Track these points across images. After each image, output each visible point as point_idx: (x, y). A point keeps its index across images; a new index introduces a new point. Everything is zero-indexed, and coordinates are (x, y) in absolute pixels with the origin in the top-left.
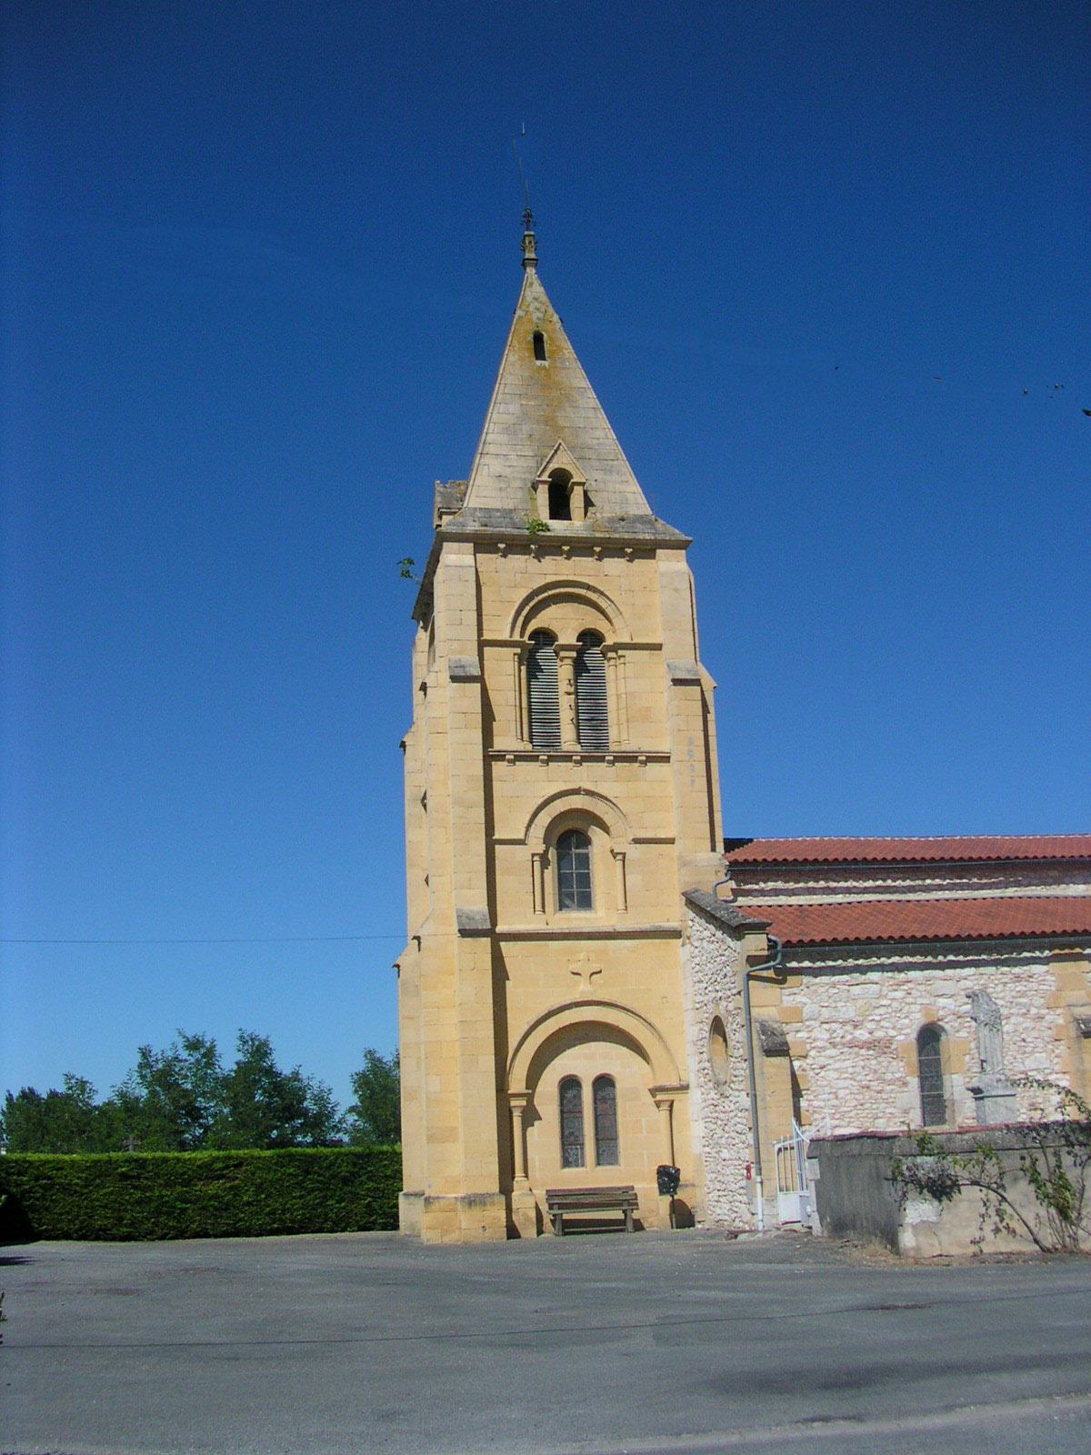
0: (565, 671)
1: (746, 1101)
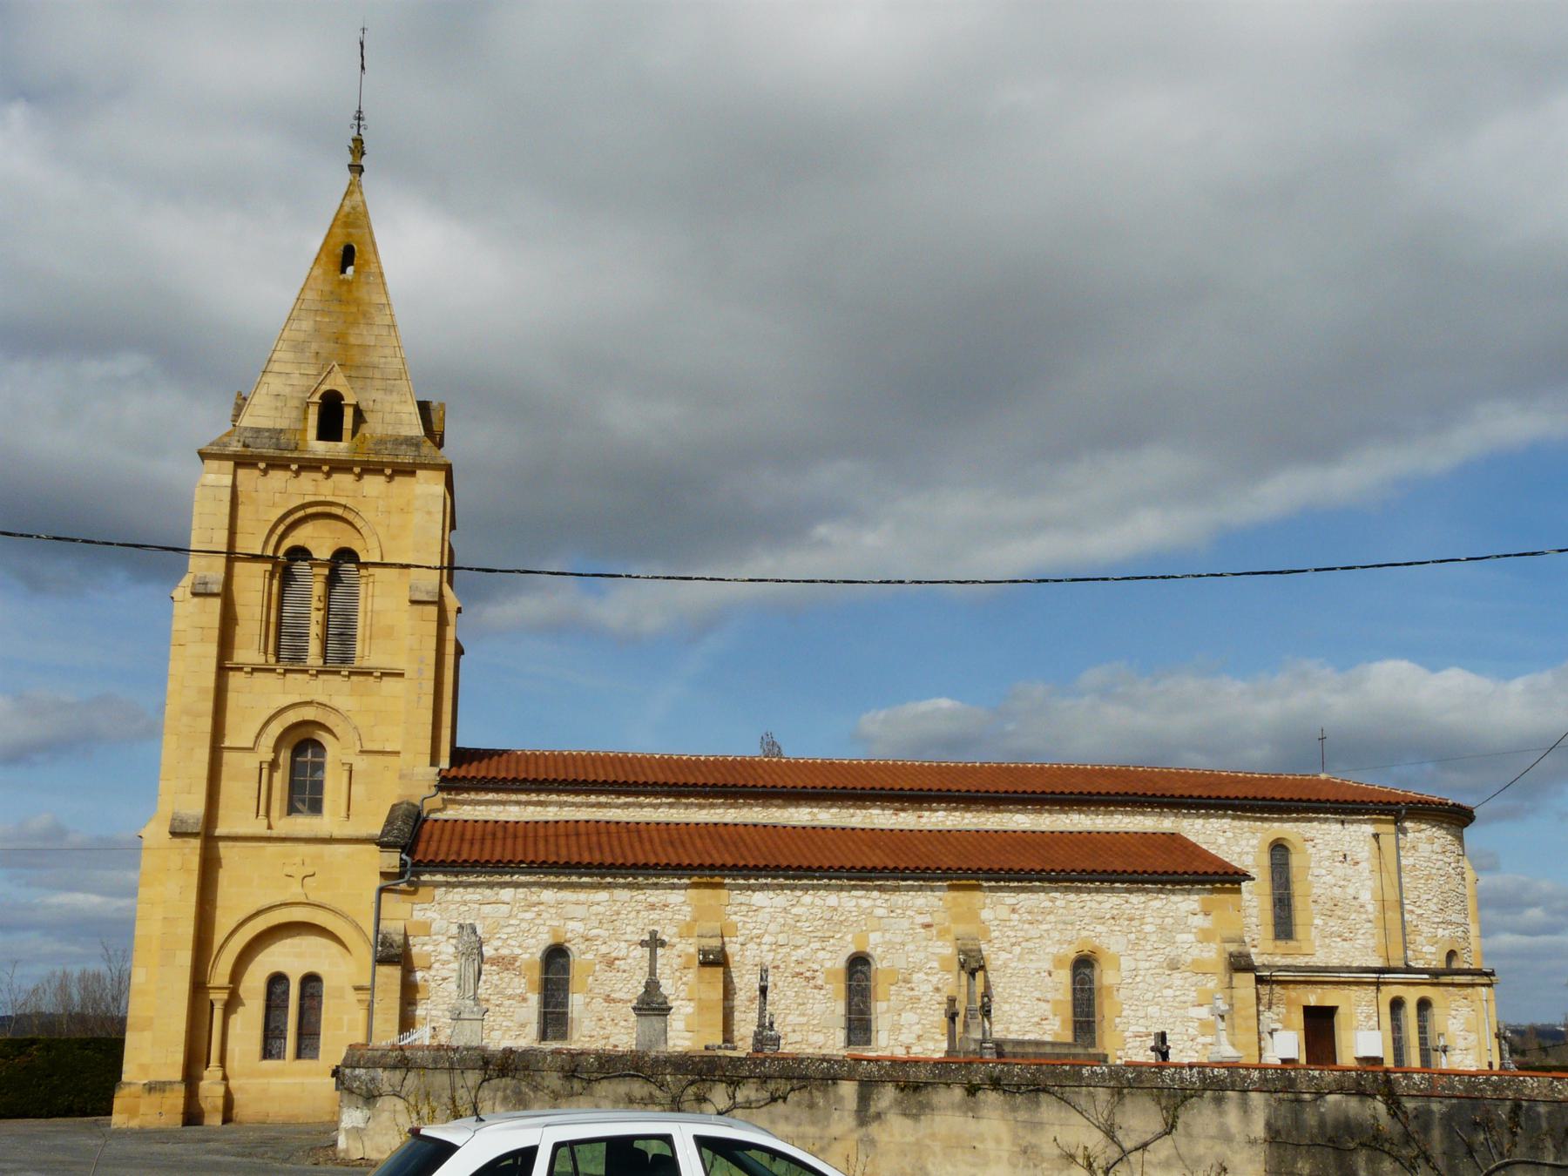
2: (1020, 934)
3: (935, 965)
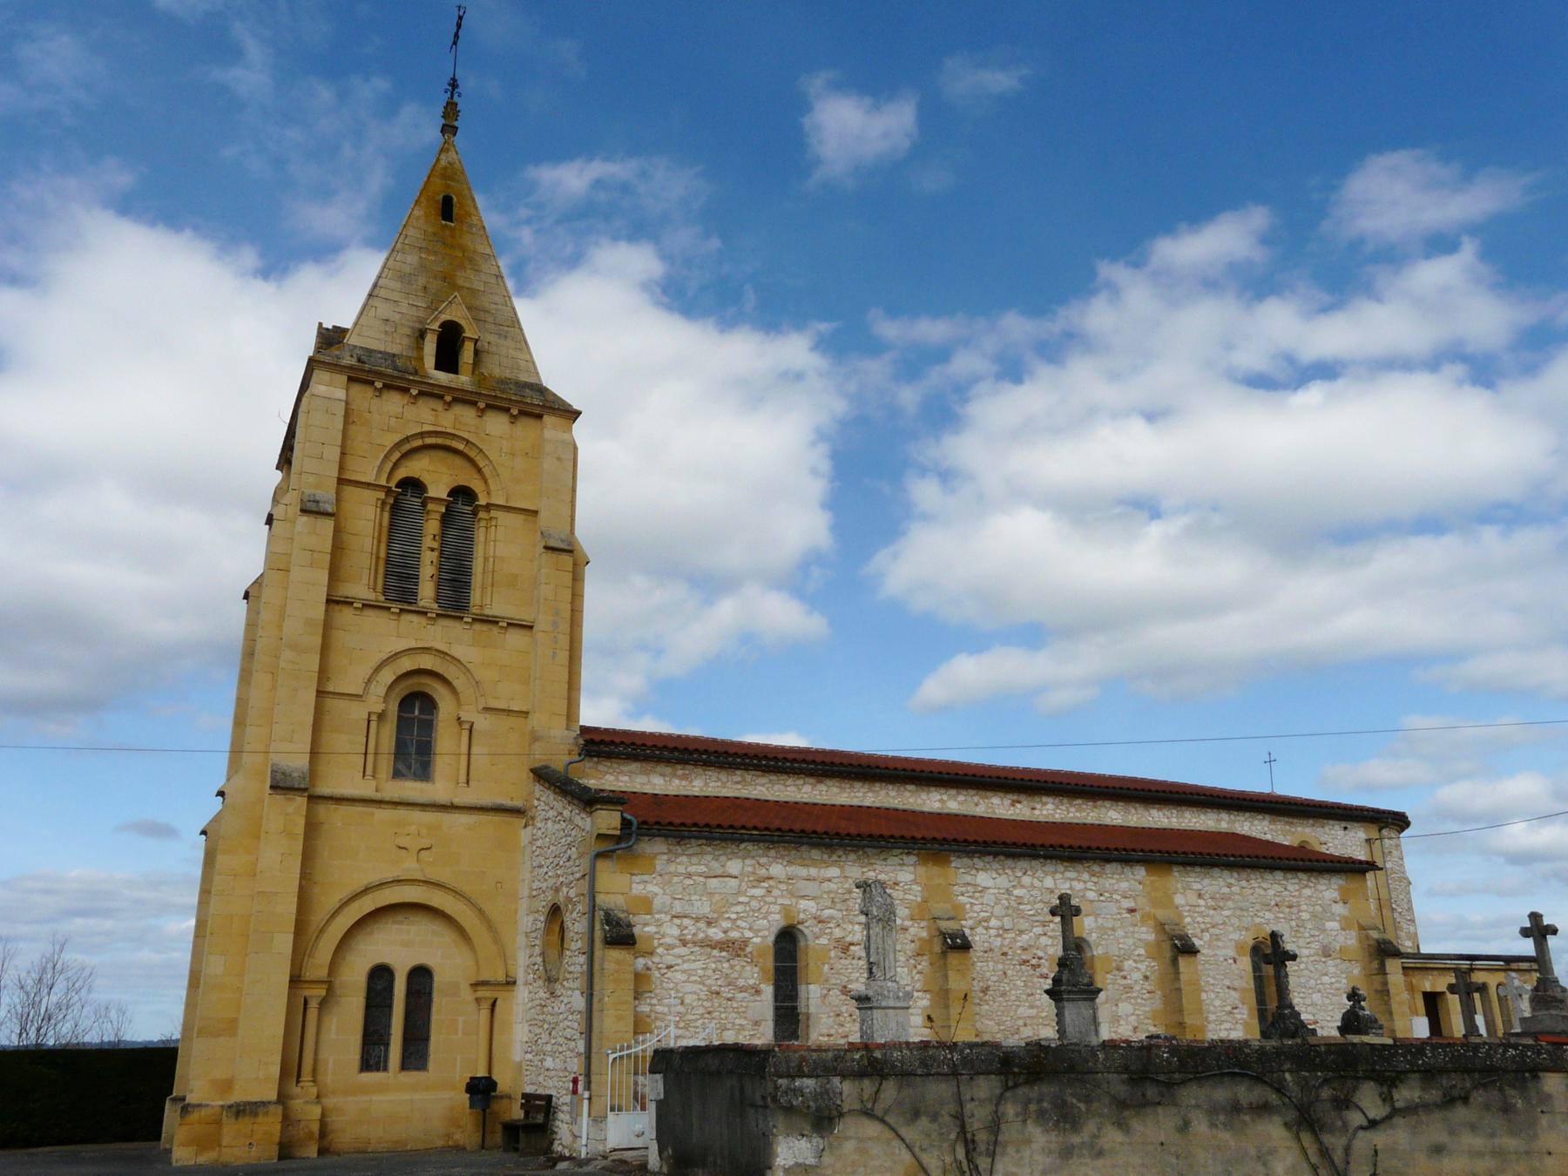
0: (432, 526)
1: (579, 1002)
2: (1208, 920)
3: (1142, 951)
